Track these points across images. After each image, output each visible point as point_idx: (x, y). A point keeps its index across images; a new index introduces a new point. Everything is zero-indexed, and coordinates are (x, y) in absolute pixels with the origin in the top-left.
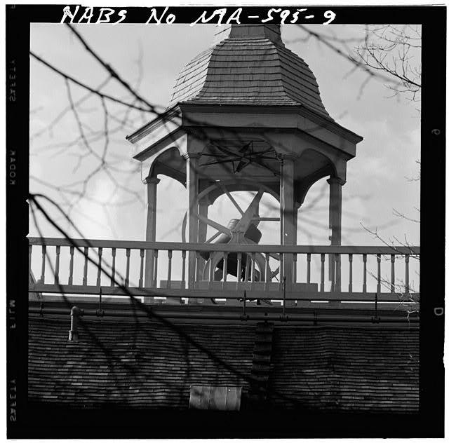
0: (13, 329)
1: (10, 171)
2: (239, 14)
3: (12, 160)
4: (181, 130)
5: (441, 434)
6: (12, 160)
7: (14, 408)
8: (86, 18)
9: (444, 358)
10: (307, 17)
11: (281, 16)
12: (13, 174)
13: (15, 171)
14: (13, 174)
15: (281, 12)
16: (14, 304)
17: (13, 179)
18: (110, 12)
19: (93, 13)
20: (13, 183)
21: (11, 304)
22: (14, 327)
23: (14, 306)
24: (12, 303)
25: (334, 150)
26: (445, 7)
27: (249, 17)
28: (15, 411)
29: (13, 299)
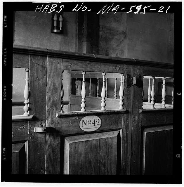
5: (181, 3)
6: (5, 90)
7: (5, 60)
8: (46, 9)
11: (137, 8)
12: (5, 96)
14: (5, 96)
16: (6, 17)
17: (5, 98)
18: (160, 11)
19: (130, 8)
22: (5, 159)
23: (6, 18)
25: (140, 137)
26: (182, 2)
27: (155, 9)
28: (6, 61)
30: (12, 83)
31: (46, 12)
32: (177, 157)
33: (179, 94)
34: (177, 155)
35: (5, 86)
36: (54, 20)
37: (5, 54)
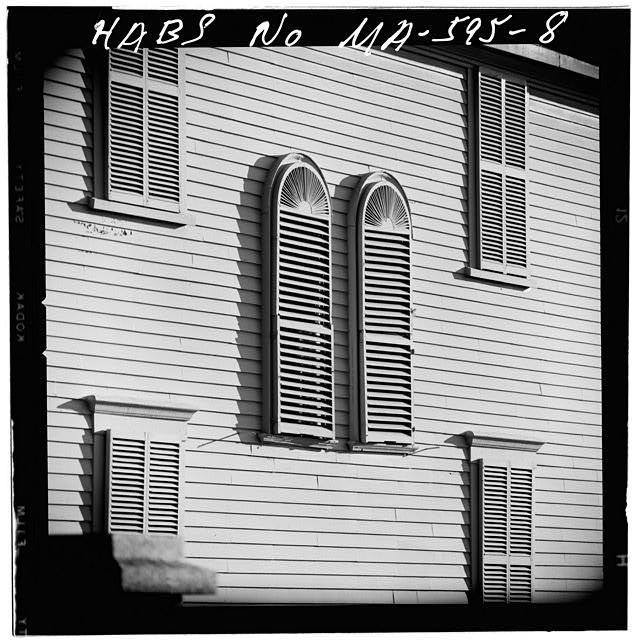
2: (376, 35)
3: (20, 307)
5: (15, 13)
6: (20, 307)
10: (511, 33)
13: (24, 322)
15: (468, 22)
16: (23, 511)
17: (21, 334)
20: (21, 339)
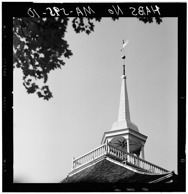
0: (38, 35)
1: (4, 105)
4: (129, 134)
5: (184, 190)
6: (4, 101)
7: (5, 71)
9: (186, 151)
21: (4, 161)
23: (5, 162)
24: (5, 27)
28: (5, 72)
29: (5, 25)
30: (12, 91)
31: (39, 17)
32: (181, 162)
33: (183, 98)
34: (182, 160)
35: (5, 97)
36: (21, 60)
37: (5, 66)
